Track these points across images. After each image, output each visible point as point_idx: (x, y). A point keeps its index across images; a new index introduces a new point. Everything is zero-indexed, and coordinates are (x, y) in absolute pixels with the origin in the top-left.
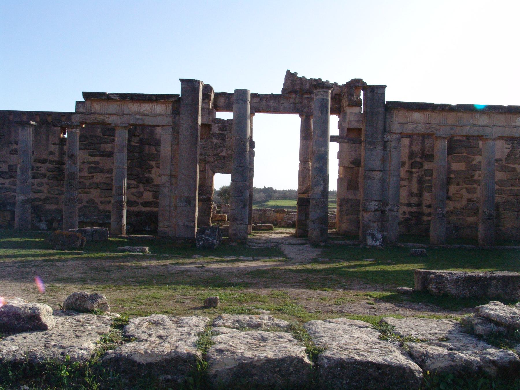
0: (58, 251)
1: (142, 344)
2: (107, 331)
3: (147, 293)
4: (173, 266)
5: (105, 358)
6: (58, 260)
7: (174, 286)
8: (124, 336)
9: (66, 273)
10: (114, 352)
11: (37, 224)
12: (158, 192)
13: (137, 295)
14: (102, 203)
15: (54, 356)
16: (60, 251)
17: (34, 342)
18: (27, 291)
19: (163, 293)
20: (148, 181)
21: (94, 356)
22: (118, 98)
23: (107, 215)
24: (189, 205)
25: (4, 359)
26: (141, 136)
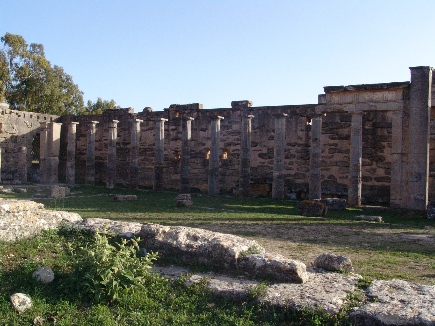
0: (305, 217)
1: (385, 306)
2: (352, 290)
3: (382, 257)
4: (405, 235)
5: (351, 314)
6: (306, 225)
7: (406, 253)
8: (368, 296)
9: (311, 236)
10: (359, 309)
11: (289, 195)
12: (390, 168)
13: (373, 259)
14: (341, 178)
15: (309, 306)
16: (307, 217)
17: (293, 292)
18: (282, 247)
19: (397, 259)
20: (380, 159)
21: (342, 311)
22: (353, 89)
23: (345, 188)
24: (420, 180)
25: (270, 302)
26: (374, 121)
